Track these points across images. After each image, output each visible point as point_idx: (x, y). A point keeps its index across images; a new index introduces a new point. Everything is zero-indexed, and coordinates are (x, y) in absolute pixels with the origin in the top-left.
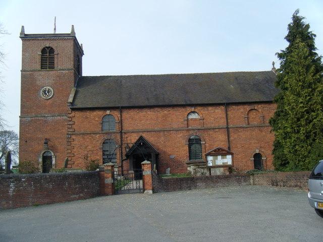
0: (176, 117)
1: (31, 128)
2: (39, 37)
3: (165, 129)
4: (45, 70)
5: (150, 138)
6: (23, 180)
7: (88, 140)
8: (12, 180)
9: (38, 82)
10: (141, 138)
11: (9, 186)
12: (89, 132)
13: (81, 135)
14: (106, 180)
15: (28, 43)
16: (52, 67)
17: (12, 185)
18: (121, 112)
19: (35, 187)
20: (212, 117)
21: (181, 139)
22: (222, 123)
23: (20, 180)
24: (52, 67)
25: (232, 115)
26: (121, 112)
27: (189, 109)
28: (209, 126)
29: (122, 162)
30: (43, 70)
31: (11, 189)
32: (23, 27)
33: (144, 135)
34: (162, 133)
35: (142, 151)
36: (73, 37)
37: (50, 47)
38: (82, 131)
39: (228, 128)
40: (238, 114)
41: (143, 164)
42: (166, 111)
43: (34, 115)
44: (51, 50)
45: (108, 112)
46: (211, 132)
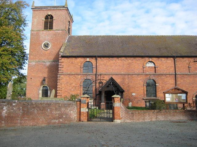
0: (137, 64)
1: (35, 69)
2: (44, 8)
3: (129, 74)
4: (46, 30)
5: (118, 80)
6: (14, 104)
7: (72, 79)
8: (5, 104)
9: (41, 39)
10: (112, 79)
11: (3, 108)
12: (74, 74)
13: (68, 75)
14: (16, 85)
15: (36, 12)
16: (51, 28)
17: (5, 108)
18: (96, 59)
19: (23, 110)
20: (165, 66)
21: (141, 81)
22: (172, 71)
23: (11, 105)
24: (51, 28)
25: (180, 65)
26: (96, 59)
27: (147, 59)
28: (162, 72)
29: (96, 96)
30: (45, 30)
31: (4, 111)
32: (34, 2)
33: (114, 77)
34: (126, 76)
35: (112, 88)
36: (66, 8)
37: (50, 15)
38: (69, 73)
39: (176, 74)
40: (183, 63)
41: (114, 98)
42: (130, 60)
43: (37, 60)
44: (52, 17)
45: (88, 59)
46: (163, 77)
